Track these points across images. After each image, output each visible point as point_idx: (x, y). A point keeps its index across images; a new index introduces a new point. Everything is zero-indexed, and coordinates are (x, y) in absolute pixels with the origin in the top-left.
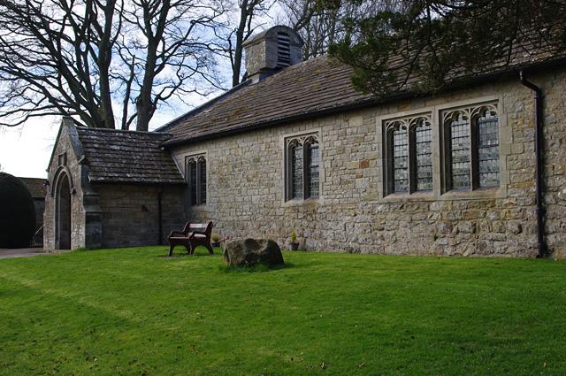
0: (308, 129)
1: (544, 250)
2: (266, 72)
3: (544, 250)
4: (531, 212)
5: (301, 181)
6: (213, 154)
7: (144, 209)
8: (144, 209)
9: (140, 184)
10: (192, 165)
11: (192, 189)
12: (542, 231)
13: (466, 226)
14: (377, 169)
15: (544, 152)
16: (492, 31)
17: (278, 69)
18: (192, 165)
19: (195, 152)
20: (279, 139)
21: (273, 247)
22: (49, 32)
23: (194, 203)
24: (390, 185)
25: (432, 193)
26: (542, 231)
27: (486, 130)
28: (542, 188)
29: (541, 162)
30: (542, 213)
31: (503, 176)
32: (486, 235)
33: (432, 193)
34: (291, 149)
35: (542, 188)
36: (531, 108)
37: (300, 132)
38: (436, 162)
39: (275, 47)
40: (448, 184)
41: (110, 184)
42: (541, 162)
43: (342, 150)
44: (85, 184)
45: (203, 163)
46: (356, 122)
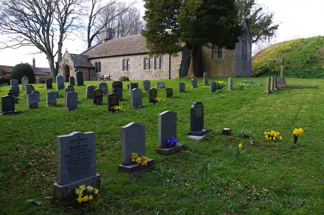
0: (128, 57)
1: (170, 78)
2: (106, 40)
3: (170, 78)
4: (168, 73)
5: (126, 67)
6: (102, 61)
7: (86, 73)
8: (86, 73)
9: (86, 67)
10: (96, 63)
11: (97, 68)
12: (170, 76)
13: (158, 75)
14: (143, 65)
15: (51, 64)
16: (175, 13)
17: (109, 39)
18: (96, 63)
19: (98, 61)
20: (121, 59)
21: (128, 78)
22: (27, 18)
23: (97, 71)
24: (145, 68)
25: (152, 69)
26: (170, 76)
27: (162, 60)
28: (170, 69)
29: (170, 65)
30: (170, 73)
31: (164, 67)
32: (161, 76)
33: (152, 69)
34: (124, 61)
35: (170, 69)
36: (169, 57)
37: (126, 58)
38: (153, 62)
39: (108, 34)
40: (155, 68)
41: (79, 67)
42: (170, 65)
43: (135, 62)
44: (75, 67)
45: (100, 63)
46: (138, 56)
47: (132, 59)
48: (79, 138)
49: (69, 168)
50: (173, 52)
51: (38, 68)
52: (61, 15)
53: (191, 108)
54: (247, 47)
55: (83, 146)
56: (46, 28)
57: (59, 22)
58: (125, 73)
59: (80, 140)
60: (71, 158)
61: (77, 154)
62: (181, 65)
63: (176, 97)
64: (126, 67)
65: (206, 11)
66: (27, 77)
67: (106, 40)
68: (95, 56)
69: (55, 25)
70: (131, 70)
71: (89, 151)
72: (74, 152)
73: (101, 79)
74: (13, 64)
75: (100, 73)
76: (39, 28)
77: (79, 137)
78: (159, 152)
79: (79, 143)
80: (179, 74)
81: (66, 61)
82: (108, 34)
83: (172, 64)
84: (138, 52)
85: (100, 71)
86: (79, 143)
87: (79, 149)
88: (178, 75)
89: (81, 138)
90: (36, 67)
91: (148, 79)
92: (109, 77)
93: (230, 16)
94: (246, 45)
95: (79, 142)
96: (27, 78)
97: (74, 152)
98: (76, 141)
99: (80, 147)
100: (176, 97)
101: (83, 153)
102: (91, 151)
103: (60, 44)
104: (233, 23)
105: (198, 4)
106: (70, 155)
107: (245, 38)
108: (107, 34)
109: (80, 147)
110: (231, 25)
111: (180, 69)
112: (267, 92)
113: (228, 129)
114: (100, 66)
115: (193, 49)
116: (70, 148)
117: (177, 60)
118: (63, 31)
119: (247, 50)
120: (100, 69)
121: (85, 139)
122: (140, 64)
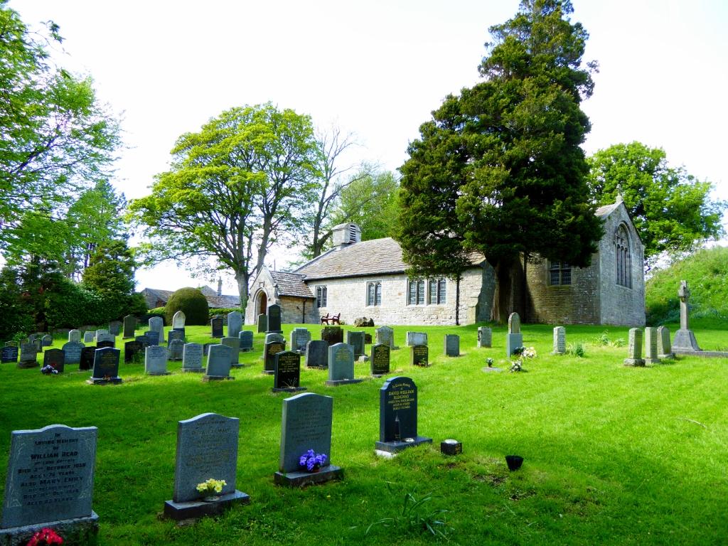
0: (378, 279)
1: (457, 324)
2: (345, 245)
3: (457, 324)
5: (374, 299)
6: (331, 288)
7: (298, 308)
10: (319, 290)
11: (319, 301)
12: (457, 318)
13: (435, 316)
14: (405, 296)
17: (350, 244)
19: (321, 285)
23: (319, 306)
24: (409, 301)
26: (457, 318)
28: (458, 305)
29: (458, 297)
30: (457, 313)
32: (440, 319)
35: (458, 305)
37: (374, 280)
39: (349, 232)
40: (429, 302)
42: (458, 297)
43: (391, 289)
45: (325, 289)
47: (386, 284)
48: (57, 438)
49: (25, 497)
50: (459, 269)
51: (225, 297)
52: (266, 199)
53: (382, 391)
54: (630, 261)
55: (64, 454)
56: (238, 222)
57: (263, 211)
58: (371, 310)
59: (59, 441)
60: (32, 477)
61: (48, 468)
62: (480, 297)
63: (648, 367)
64: (374, 299)
65: (514, 189)
66: (183, 314)
67: (345, 245)
68: (318, 276)
69: (256, 216)
70: (381, 306)
71: (77, 466)
72: (41, 465)
73: (323, 320)
74: (174, 289)
75: (324, 308)
76: (224, 222)
77: (58, 435)
78: (279, 481)
79: (55, 448)
80: (474, 316)
81: (262, 285)
82: (349, 234)
83: (461, 294)
84: (396, 270)
85: (325, 304)
86: (55, 448)
87: (55, 459)
88: (474, 318)
89: (63, 437)
90: (136, 291)
91: (389, 325)
92: (338, 317)
93: (569, 198)
94: (630, 257)
95: (56, 445)
96: (183, 315)
97: (41, 465)
98: (49, 442)
99: (56, 455)
100: (648, 367)
101: (62, 467)
102: (84, 465)
103: (263, 252)
104: (576, 213)
105: (497, 177)
106: (29, 471)
107: (625, 241)
108: (346, 234)
109: (56, 455)
110: (573, 217)
111: (478, 307)
112: (632, 361)
113: (455, 442)
114: (325, 296)
115: (498, 264)
116: (33, 457)
117: (473, 285)
118: (268, 227)
119: (630, 266)
120: (325, 300)
121: (73, 440)
122: (400, 294)
